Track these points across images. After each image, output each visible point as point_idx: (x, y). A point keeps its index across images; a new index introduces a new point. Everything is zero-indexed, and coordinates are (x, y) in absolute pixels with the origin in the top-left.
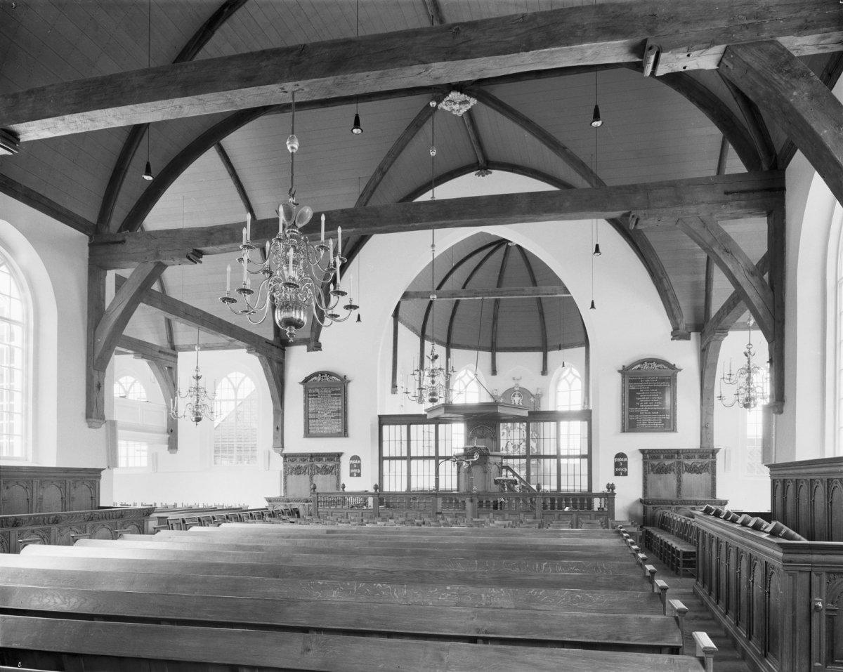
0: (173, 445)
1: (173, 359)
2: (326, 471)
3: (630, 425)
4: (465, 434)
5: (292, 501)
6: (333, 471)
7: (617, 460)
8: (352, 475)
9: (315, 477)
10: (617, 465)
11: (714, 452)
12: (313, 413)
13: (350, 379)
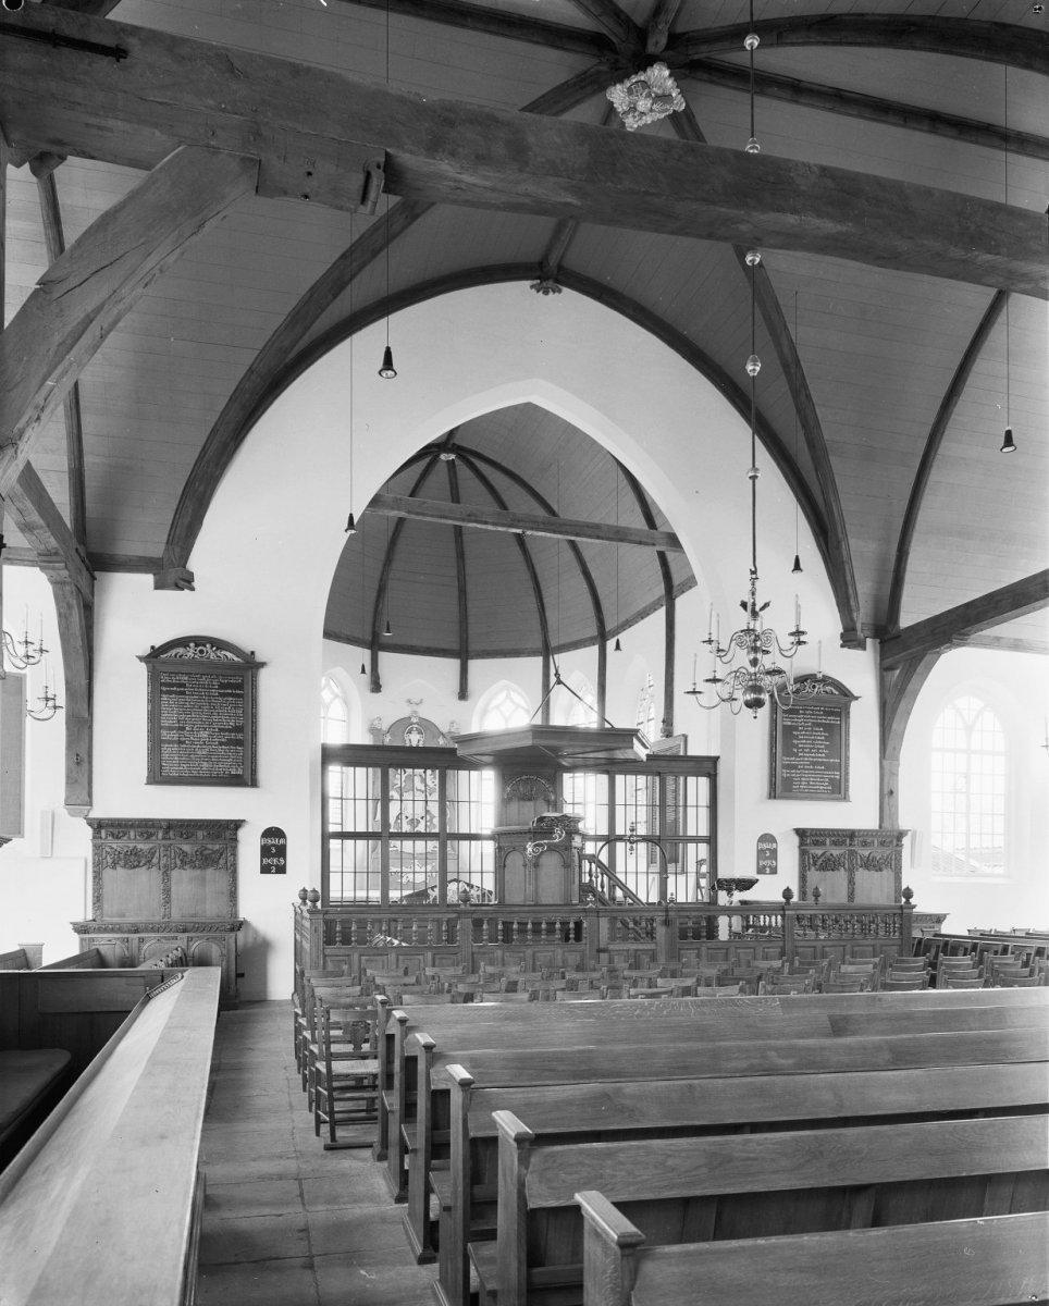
3: (780, 787)
5: (146, 930)
6: (222, 861)
7: (265, 841)
8: (265, 869)
10: (761, 853)
11: (901, 835)
12: (170, 729)
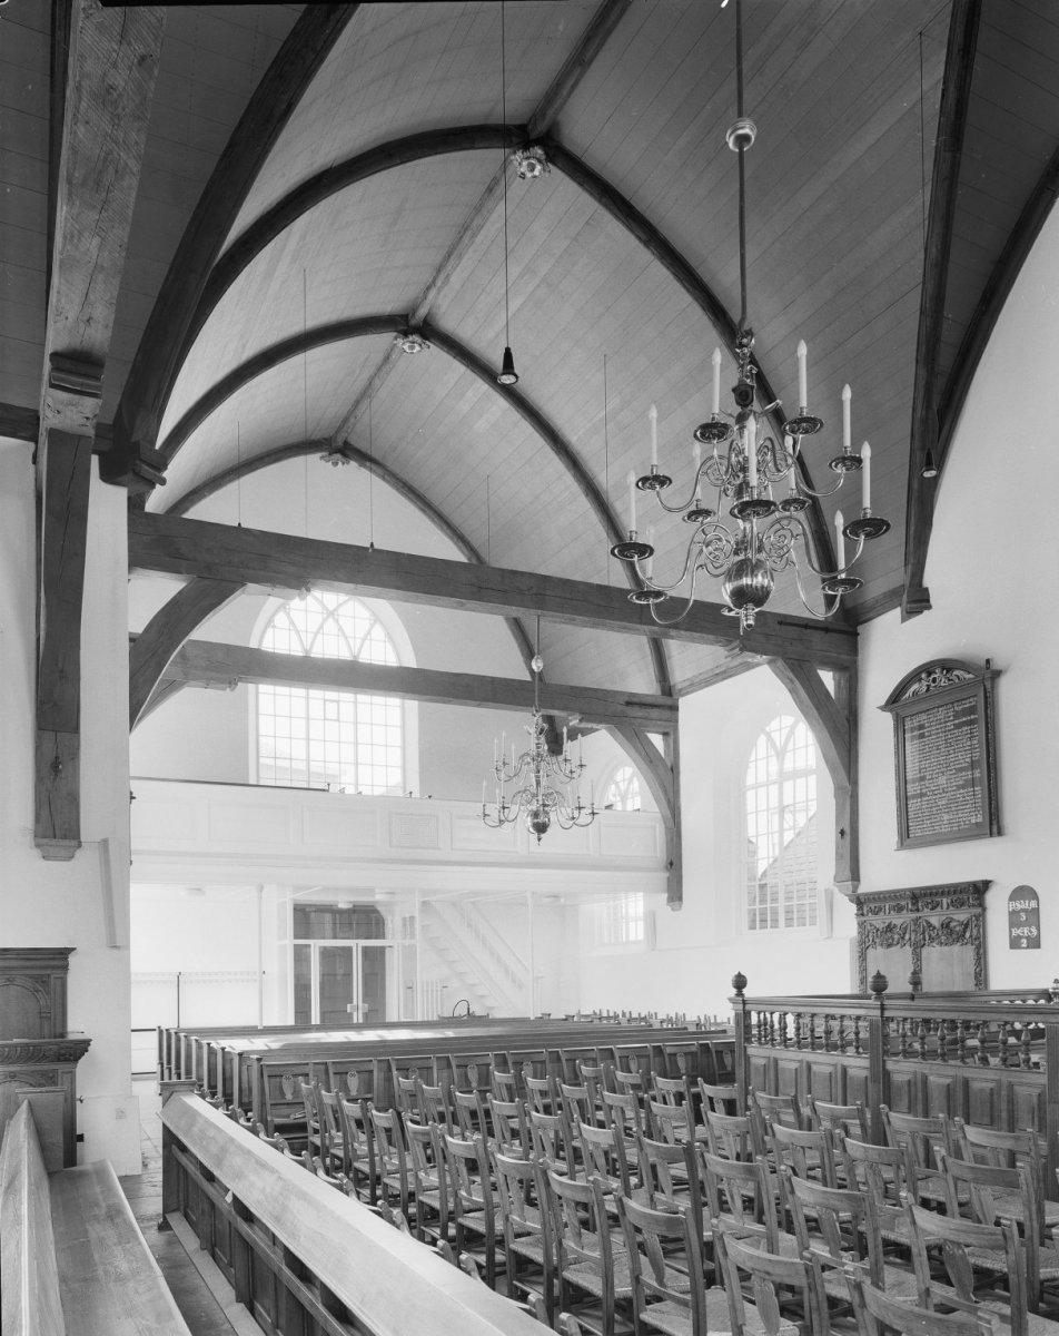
0: (675, 893)
1: (666, 714)
2: (952, 934)
4: (290, 686)
6: (968, 935)
8: (1015, 943)
9: (925, 951)
13: (999, 668)
